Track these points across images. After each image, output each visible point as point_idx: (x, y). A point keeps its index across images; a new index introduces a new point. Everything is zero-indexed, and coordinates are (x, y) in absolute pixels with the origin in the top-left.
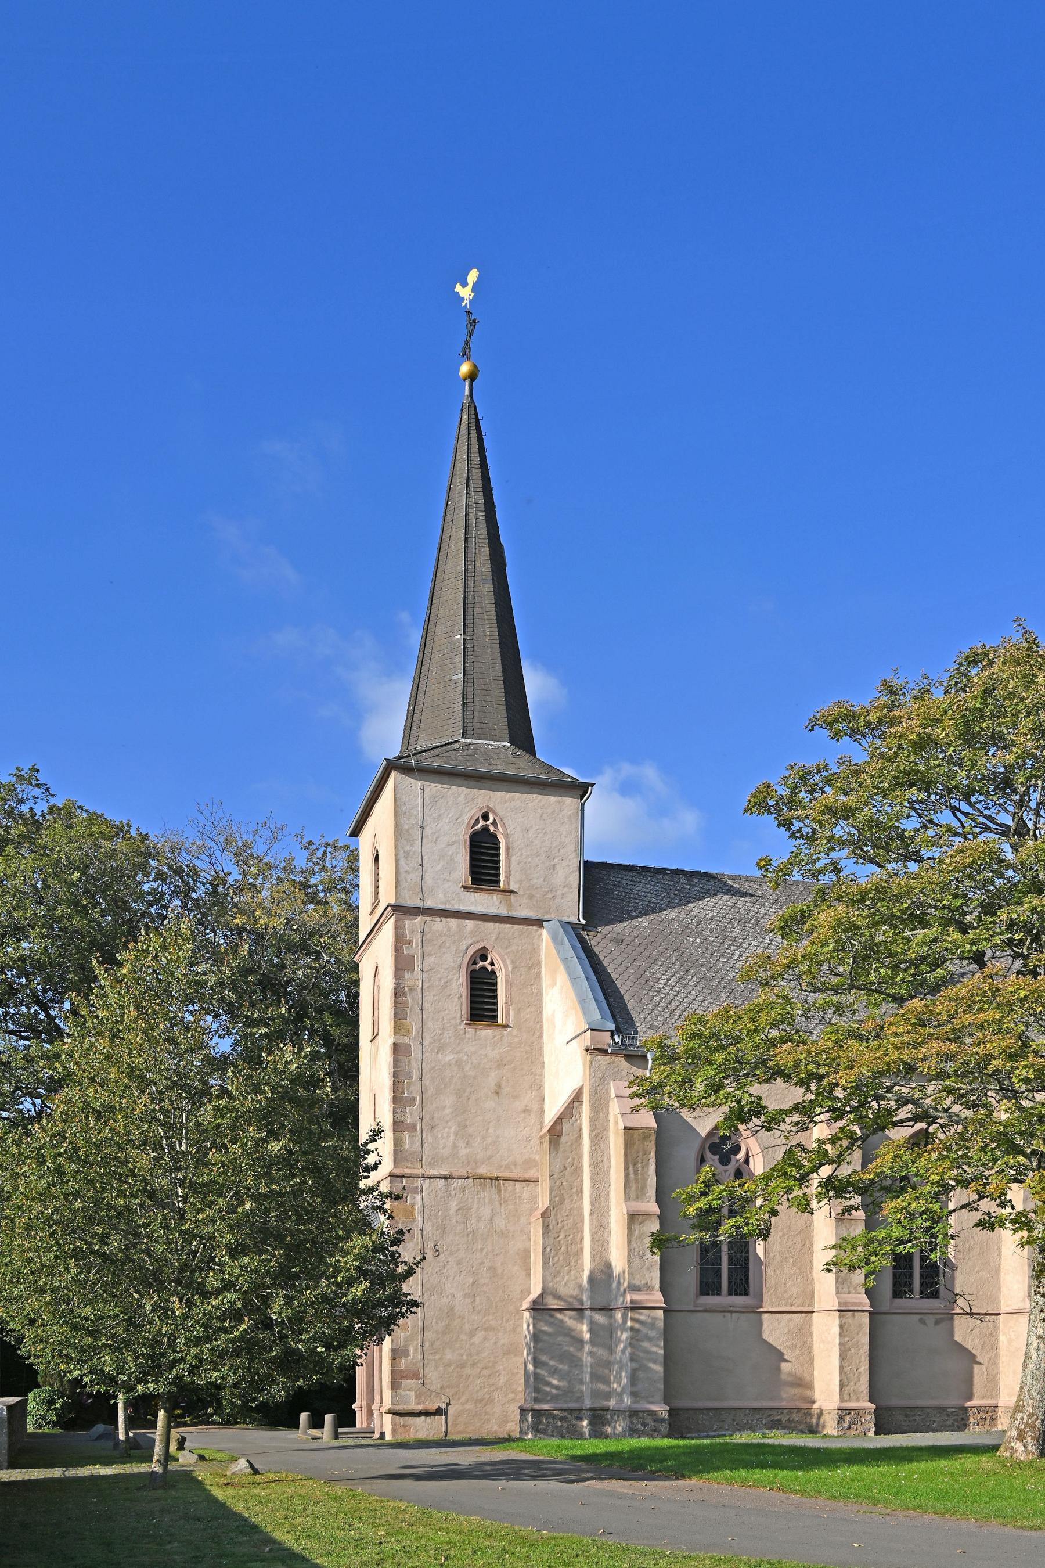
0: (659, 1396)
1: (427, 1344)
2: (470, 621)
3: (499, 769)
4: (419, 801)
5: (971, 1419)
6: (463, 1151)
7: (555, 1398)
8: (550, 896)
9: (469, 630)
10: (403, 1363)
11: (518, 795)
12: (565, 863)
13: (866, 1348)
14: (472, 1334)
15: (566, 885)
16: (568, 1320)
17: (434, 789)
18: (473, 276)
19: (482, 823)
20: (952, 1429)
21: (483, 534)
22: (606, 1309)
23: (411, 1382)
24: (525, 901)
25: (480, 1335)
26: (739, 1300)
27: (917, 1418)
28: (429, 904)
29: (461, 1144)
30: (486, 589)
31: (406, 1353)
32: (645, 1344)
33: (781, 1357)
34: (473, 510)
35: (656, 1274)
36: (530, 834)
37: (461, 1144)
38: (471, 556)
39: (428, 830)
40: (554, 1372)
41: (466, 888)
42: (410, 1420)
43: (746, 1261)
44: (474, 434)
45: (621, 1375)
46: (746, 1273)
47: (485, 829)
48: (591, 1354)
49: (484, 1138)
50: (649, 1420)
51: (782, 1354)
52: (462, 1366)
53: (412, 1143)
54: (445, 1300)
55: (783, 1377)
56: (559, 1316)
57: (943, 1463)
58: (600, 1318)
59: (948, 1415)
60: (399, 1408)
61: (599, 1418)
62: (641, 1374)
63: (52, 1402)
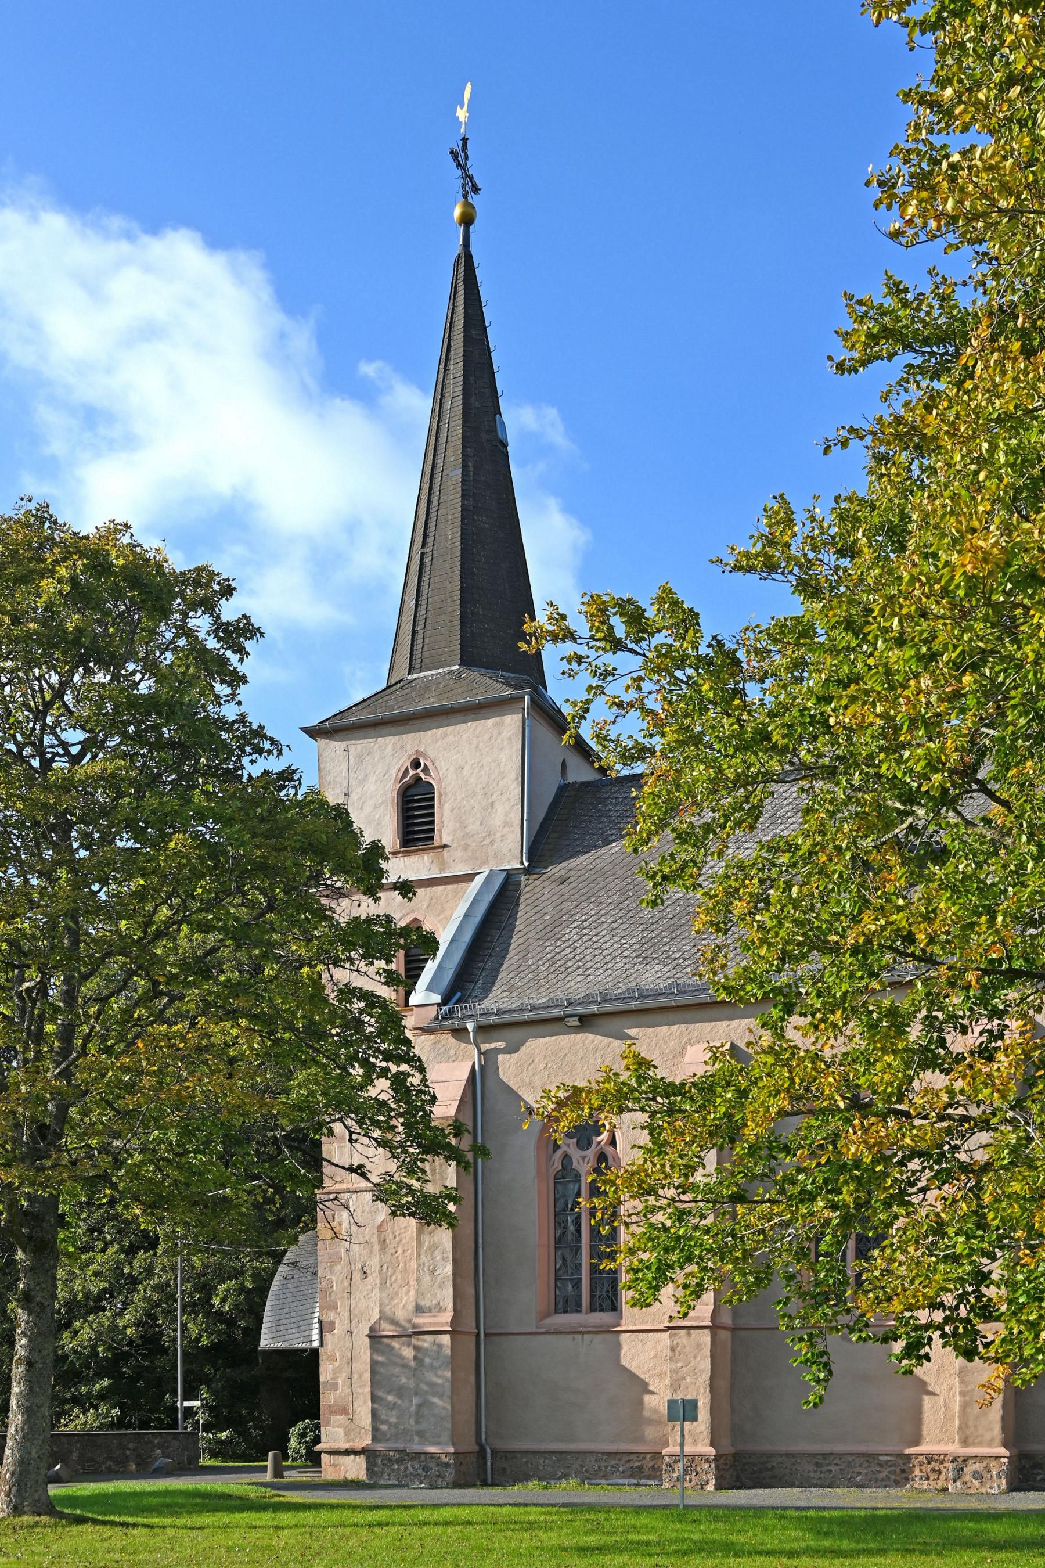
0: (445, 1437)
1: (355, 1376)
4: (343, 767)
5: (917, 1472)
8: (488, 841)
9: (430, 540)
11: (450, 728)
12: (504, 798)
13: (707, 1375)
15: (506, 824)
17: (359, 747)
19: (412, 772)
20: (885, 1483)
23: (341, 1419)
24: (459, 854)
27: (833, 1468)
33: (644, 1388)
35: (449, 1291)
36: (465, 772)
51: (647, 1384)
55: (646, 1413)
56: (395, 1344)
59: (881, 1465)
62: (426, 1411)
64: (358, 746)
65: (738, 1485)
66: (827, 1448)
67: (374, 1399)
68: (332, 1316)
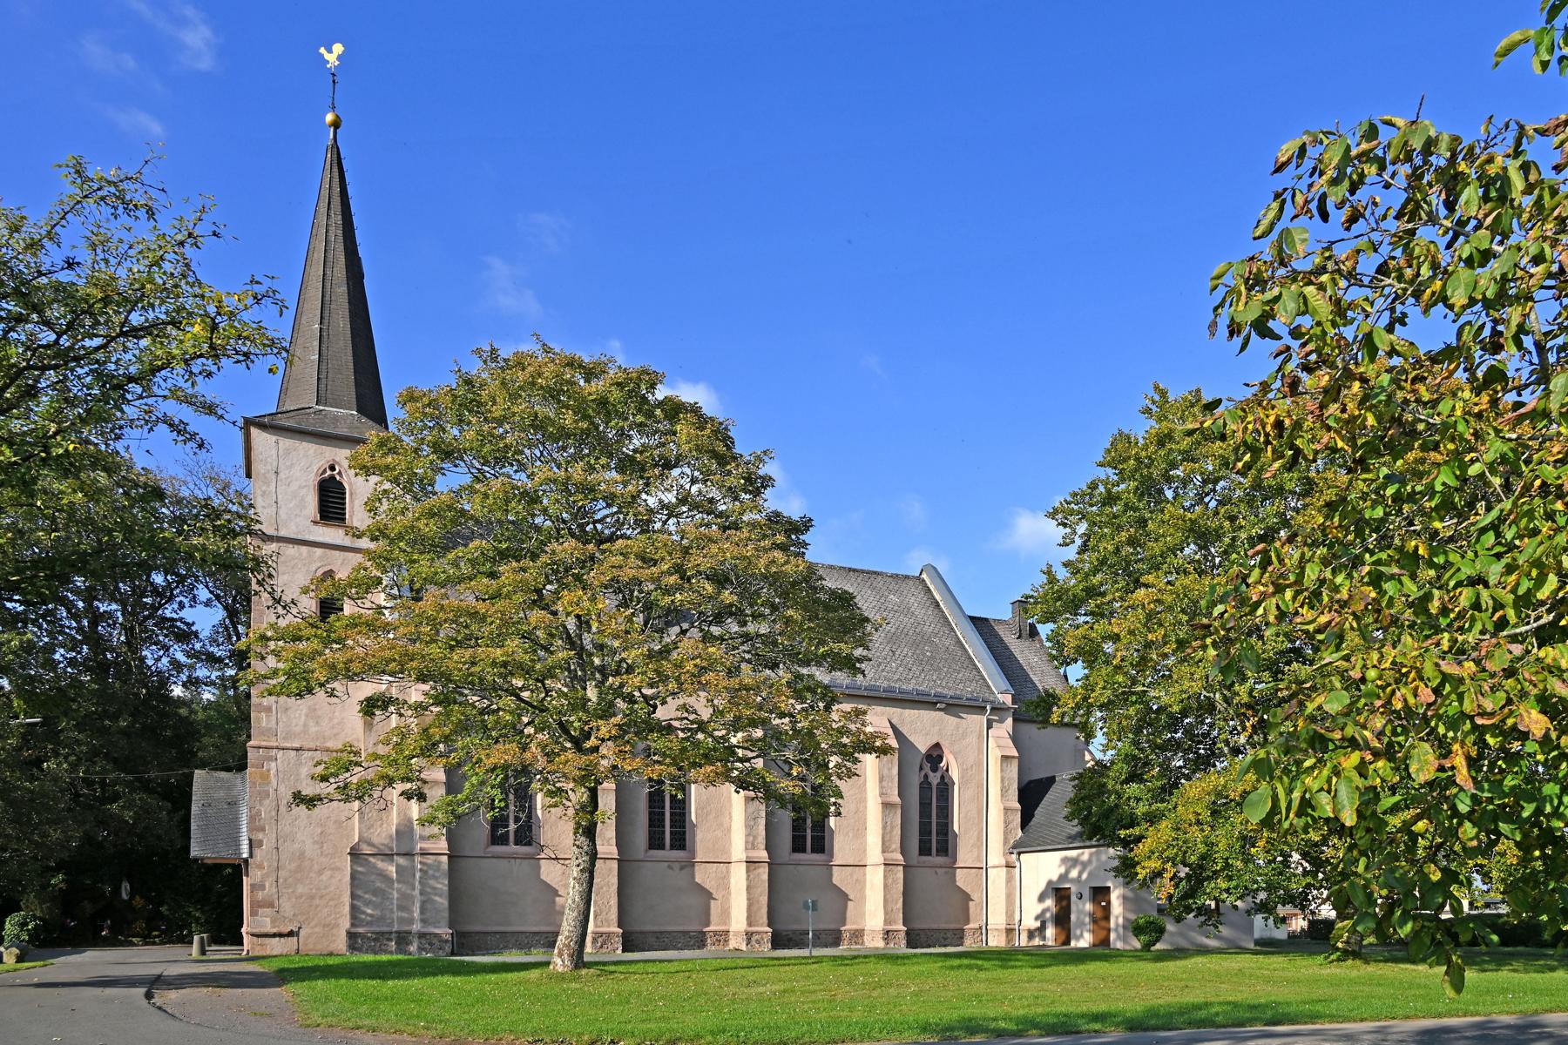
0: (445, 922)
2: (326, 314)
3: (343, 431)
4: (274, 452)
6: (313, 729)
7: (369, 924)
10: (260, 895)
13: (616, 887)
14: (320, 872)
16: (380, 864)
18: (338, 48)
21: (340, 247)
22: (409, 855)
23: (268, 911)
25: (328, 873)
26: (940, 860)
28: (283, 533)
29: (311, 723)
30: (341, 291)
31: (262, 887)
32: (432, 882)
33: (555, 893)
34: (332, 229)
37: (311, 723)
38: (329, 264)
39: (282, 475)
40: (368, 903)
41: (315, 522)
42: (267, 940)
43: (946, 834)
44: (336, 170)
45: (421, 907)
46: (946, 841)
47: (332, 478)
48: (398, 890)
49: (331, 719)
50: (435, 941)
52: (312, 898)
53: (268, 721)
54: (296, 846)
56: (371, 859)
57: (510, 976)
58: (401, 861)
60: (256, 931)
61: (403, 939)
63: (26, 924)
64: (286, 443)
65: (784, 947)
66: (662, 929)
67: (353, 896)
68: (260, 836)
